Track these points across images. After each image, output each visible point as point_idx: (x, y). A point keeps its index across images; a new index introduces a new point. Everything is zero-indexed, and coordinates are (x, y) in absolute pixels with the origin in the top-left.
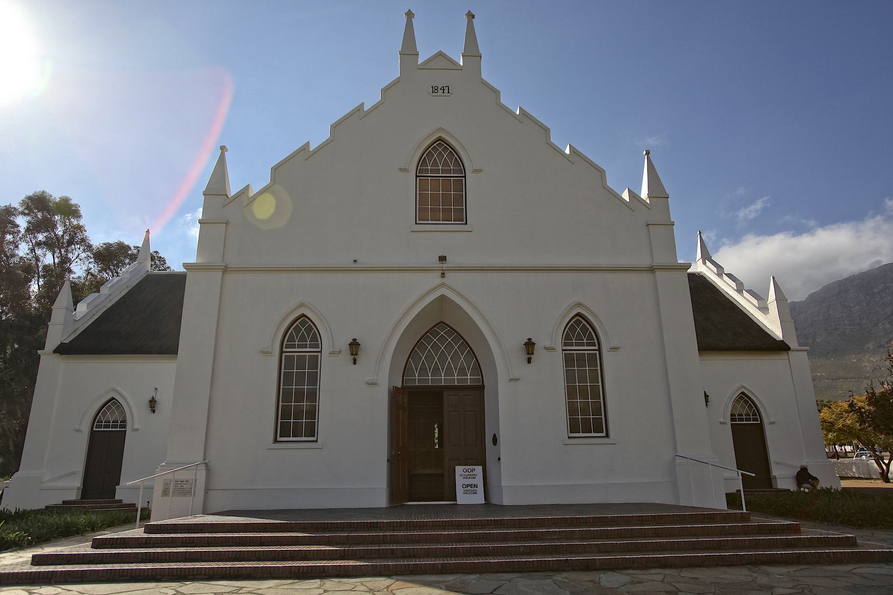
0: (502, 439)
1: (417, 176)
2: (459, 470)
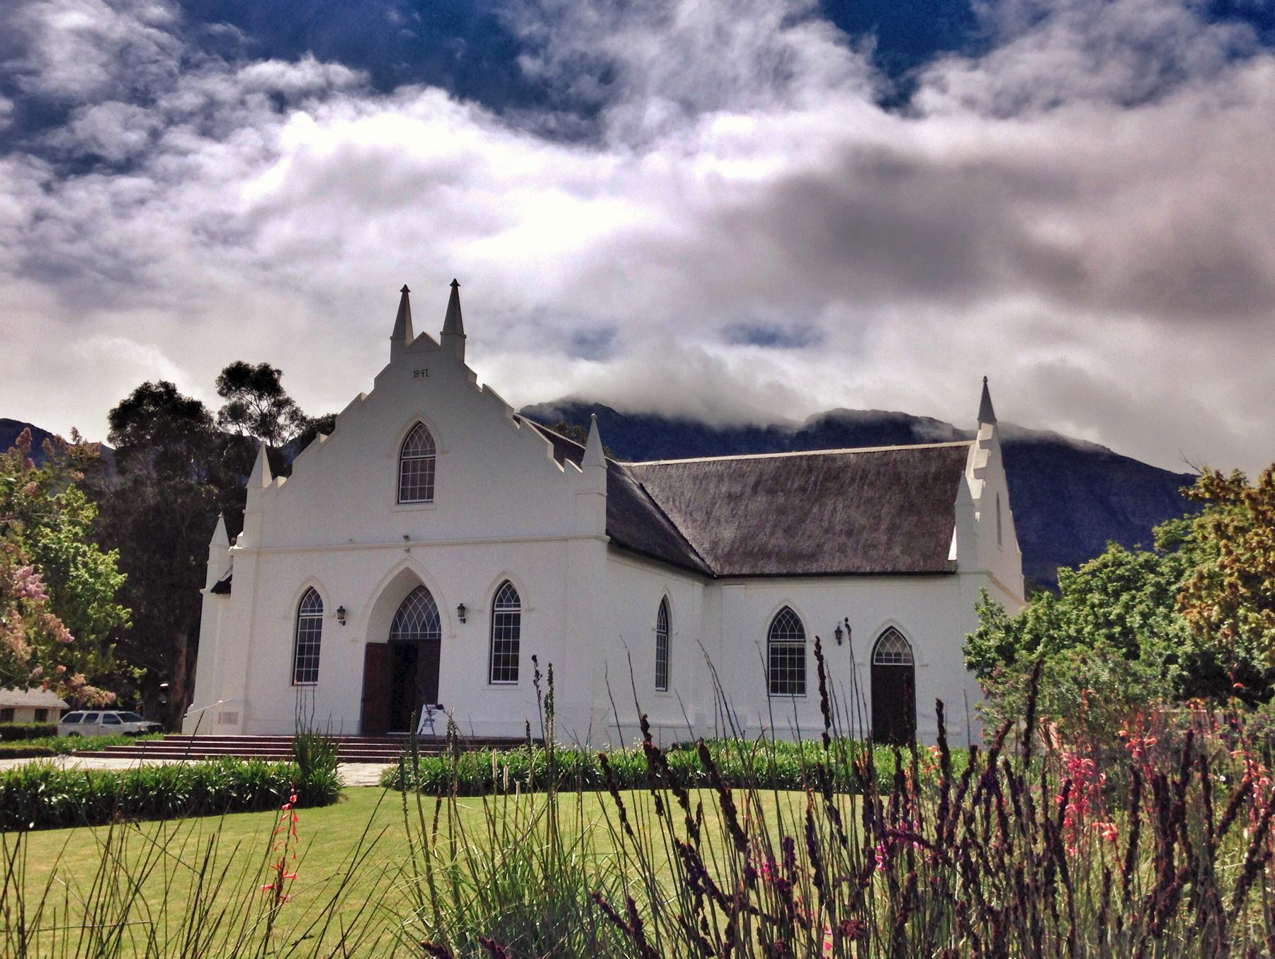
1: (401, 459)
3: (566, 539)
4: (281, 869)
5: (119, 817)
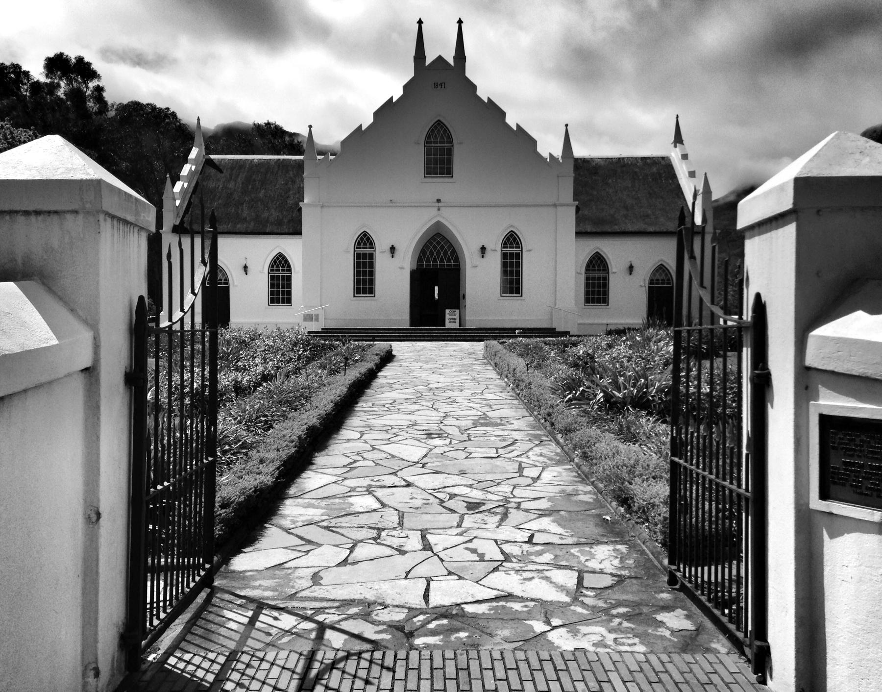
0: (467, 297)
1: (425, 146)
2: (447, 311)
5: (635, 399)
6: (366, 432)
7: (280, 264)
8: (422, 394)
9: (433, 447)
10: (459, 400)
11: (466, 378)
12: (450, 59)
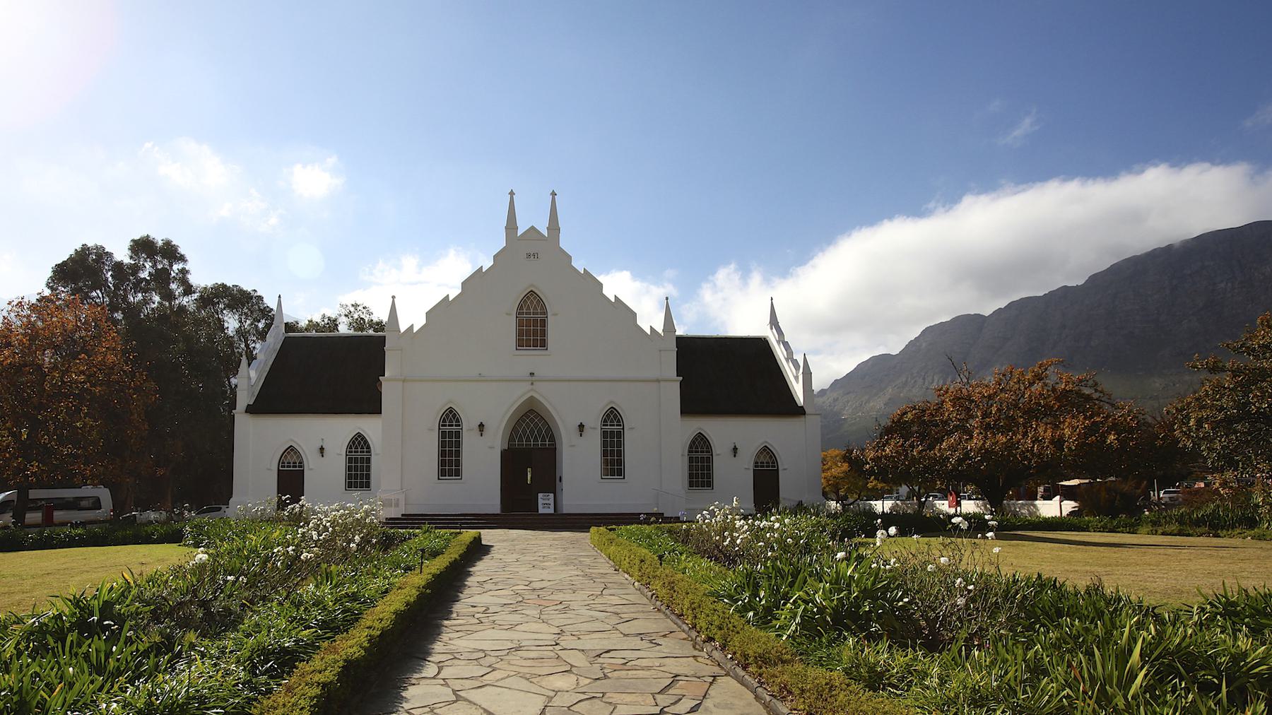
0: (563, 479)
1: (517, 317)
2: (540, 495)
3: (658, 381)
4: (67, 599)
6: (446, 663)
7: (359, 444)
8: (523, 598)
9: (552, 694)
10: (574, 605)
11: (576, 573)
12: (543, 230)
